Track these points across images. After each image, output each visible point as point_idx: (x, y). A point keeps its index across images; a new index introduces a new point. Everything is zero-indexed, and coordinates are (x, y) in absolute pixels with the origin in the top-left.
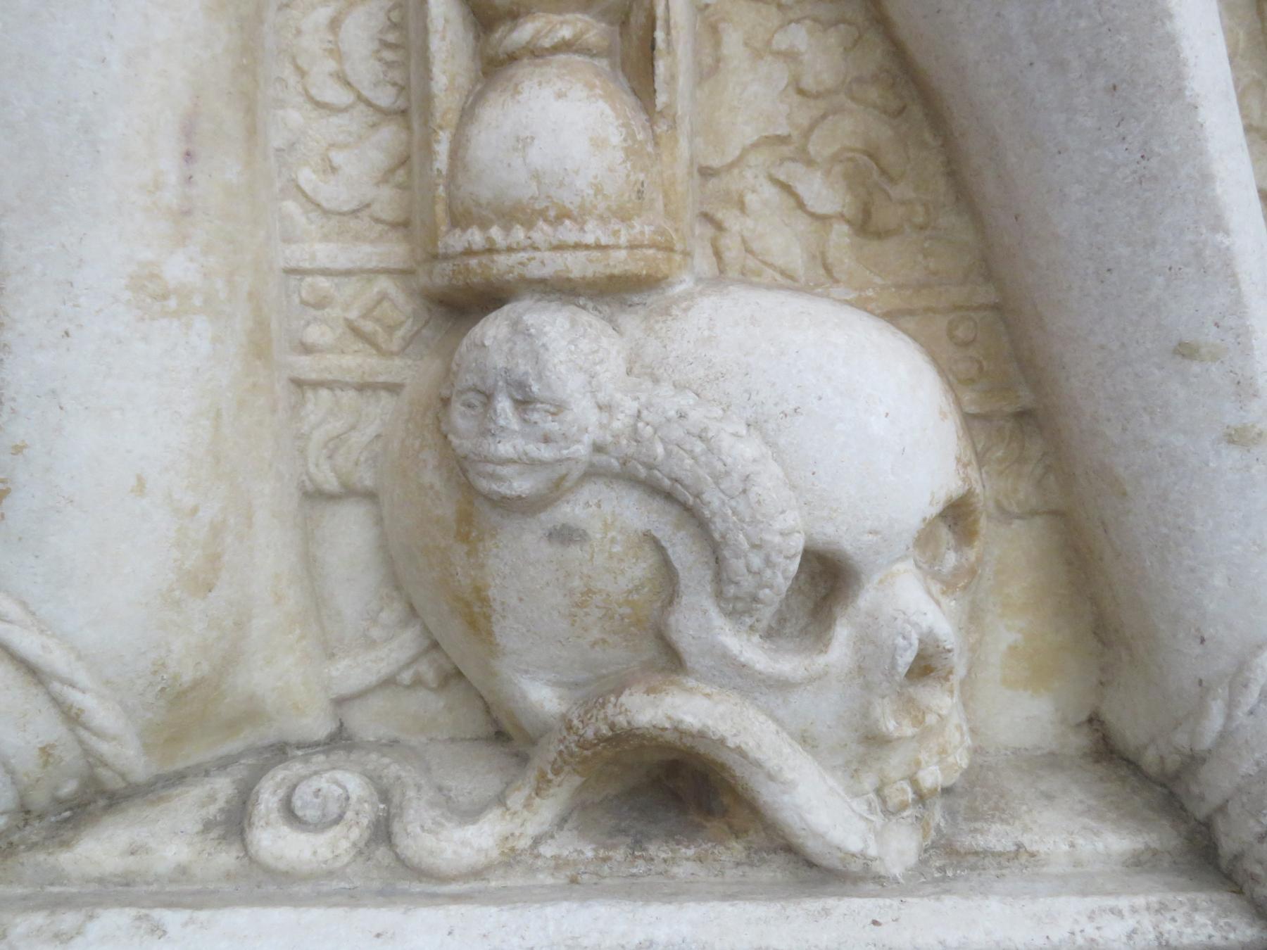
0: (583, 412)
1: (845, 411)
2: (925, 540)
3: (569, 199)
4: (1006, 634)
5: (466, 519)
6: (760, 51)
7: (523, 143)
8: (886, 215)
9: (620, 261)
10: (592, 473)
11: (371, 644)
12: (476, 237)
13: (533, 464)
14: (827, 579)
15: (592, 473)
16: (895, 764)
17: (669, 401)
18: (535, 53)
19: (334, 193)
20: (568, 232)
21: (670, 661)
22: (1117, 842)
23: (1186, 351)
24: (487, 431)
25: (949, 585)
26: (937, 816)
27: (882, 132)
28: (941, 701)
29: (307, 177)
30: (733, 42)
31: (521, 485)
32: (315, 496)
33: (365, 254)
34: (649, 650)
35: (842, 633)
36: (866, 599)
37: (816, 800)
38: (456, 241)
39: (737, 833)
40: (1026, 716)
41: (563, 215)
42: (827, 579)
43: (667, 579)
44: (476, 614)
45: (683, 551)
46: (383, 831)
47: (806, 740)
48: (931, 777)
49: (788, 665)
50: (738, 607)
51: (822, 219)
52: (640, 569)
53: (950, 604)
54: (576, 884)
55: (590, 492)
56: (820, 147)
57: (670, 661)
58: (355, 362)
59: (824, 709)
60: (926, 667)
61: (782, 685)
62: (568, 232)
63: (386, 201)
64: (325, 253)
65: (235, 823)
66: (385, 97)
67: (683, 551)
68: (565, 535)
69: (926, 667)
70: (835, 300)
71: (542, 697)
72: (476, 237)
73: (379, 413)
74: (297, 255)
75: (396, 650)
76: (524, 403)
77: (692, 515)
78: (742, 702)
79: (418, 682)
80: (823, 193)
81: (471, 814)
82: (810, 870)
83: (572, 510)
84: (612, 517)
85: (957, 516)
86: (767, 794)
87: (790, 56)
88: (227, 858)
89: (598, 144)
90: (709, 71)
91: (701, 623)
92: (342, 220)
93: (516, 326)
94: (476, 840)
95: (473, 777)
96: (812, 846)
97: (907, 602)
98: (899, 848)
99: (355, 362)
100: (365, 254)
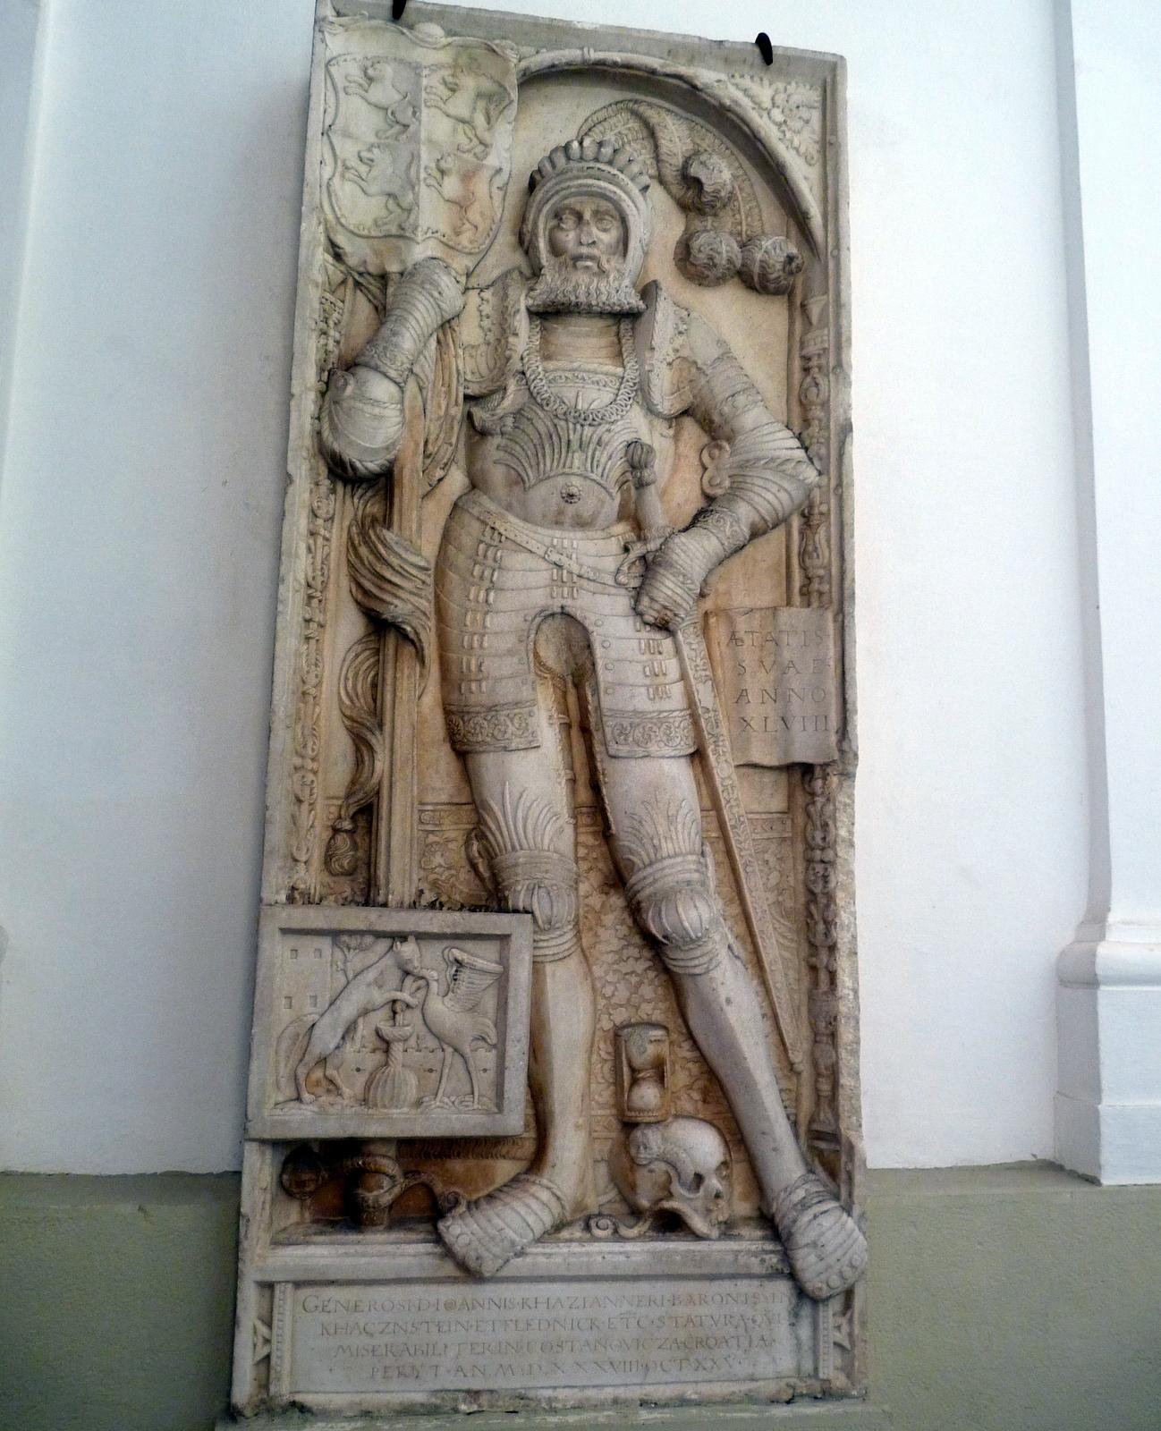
0: (655, 1149)
1: (701, 1145)
2: (718, 1169)
3: (651, 1107)
4: (738, 1189)
5: (632, 1168)
6: (683, 1068)
7: (642, 1097)
8: (709, 1099)
9: (660, 1118)
10: (656, 1159)
11: (606, 1193)
12: (633, 1114)
13: (646, 1158)
14: (699, 1178)
15: (656, 1159)
16: (713, 1216)
17: (669, 1147)
18: (643, 1079)
19: (601, 1100)
20: (650, 1114)
21: (670, 1196)
22: (759, 1233)
23: (763, 1133)
24: (638, 1153)
25: (724, 1178)
26: (723, 1227)
27: (707, 1083)
28: (722, 1203)
29: (596, 1097)
30: (677, 1067)
31: (644, 1162)
32: (596, 1161)
33: (608, 1112)
34: (666, 1193)
35: (702, 1189)
36: (706, 1182)
37: (698, 1223)
38: (629, 1114)
39: (682, 1230)
40: (743, 1208)
41: (396, 661)
42: (699, 1178)
43: (669, 1180)
44: (633, 1187)
45: (672, 1173)
46: (616, 1231)
47: (696, 1210)
48: (721, 1218)
49: (692, 1196)
50: (682, 1185)
51: (696, 1101)
52: (664, 1178)
53: (724, 1183)
54: (652, 1239)
55: (656, 1163)
56: (696, 1086)
57: (670, 1196)
58: (605, 1134)
59: (699, 1204)
60: (718, 1196)
61: (691, 1199)
62: (650, 1114)
63: (612, 1101)
64: (600, 1112)
65: (587, 1228)
66: (611, 1080)
67: (672, 1173)
68: (651, 1171)
69: (718, 1196)
70: (700, 1119)
71: (644, 1202)
72: (633, 1114)
73: (609, 1144)
74: (593, 1113)
75: (612, 1194)
76: (646, 1148)
77: (675, 1168)
78: (682, 1202)
79: (615, 1202)
80: (696, 1096)
81: (632, 1227)
82: (698, 1237)
83: (652, 1166)
84: (660, 1167)
85: (725, 1164)
86: (689, 1221)
87: (689, 1069)
88: (588, 1236)
89: (655, 1096)
90: (673, 1072)
91: (676, 1188)
92: (602, 1106)
93: (643, 1134)
94: (634, 1232)
95: (631, 1221)
96: (697, 1232)
97: (714, 1183)
98: (715, 1233)
99: (605, 1134)
100: (608, 1112)
